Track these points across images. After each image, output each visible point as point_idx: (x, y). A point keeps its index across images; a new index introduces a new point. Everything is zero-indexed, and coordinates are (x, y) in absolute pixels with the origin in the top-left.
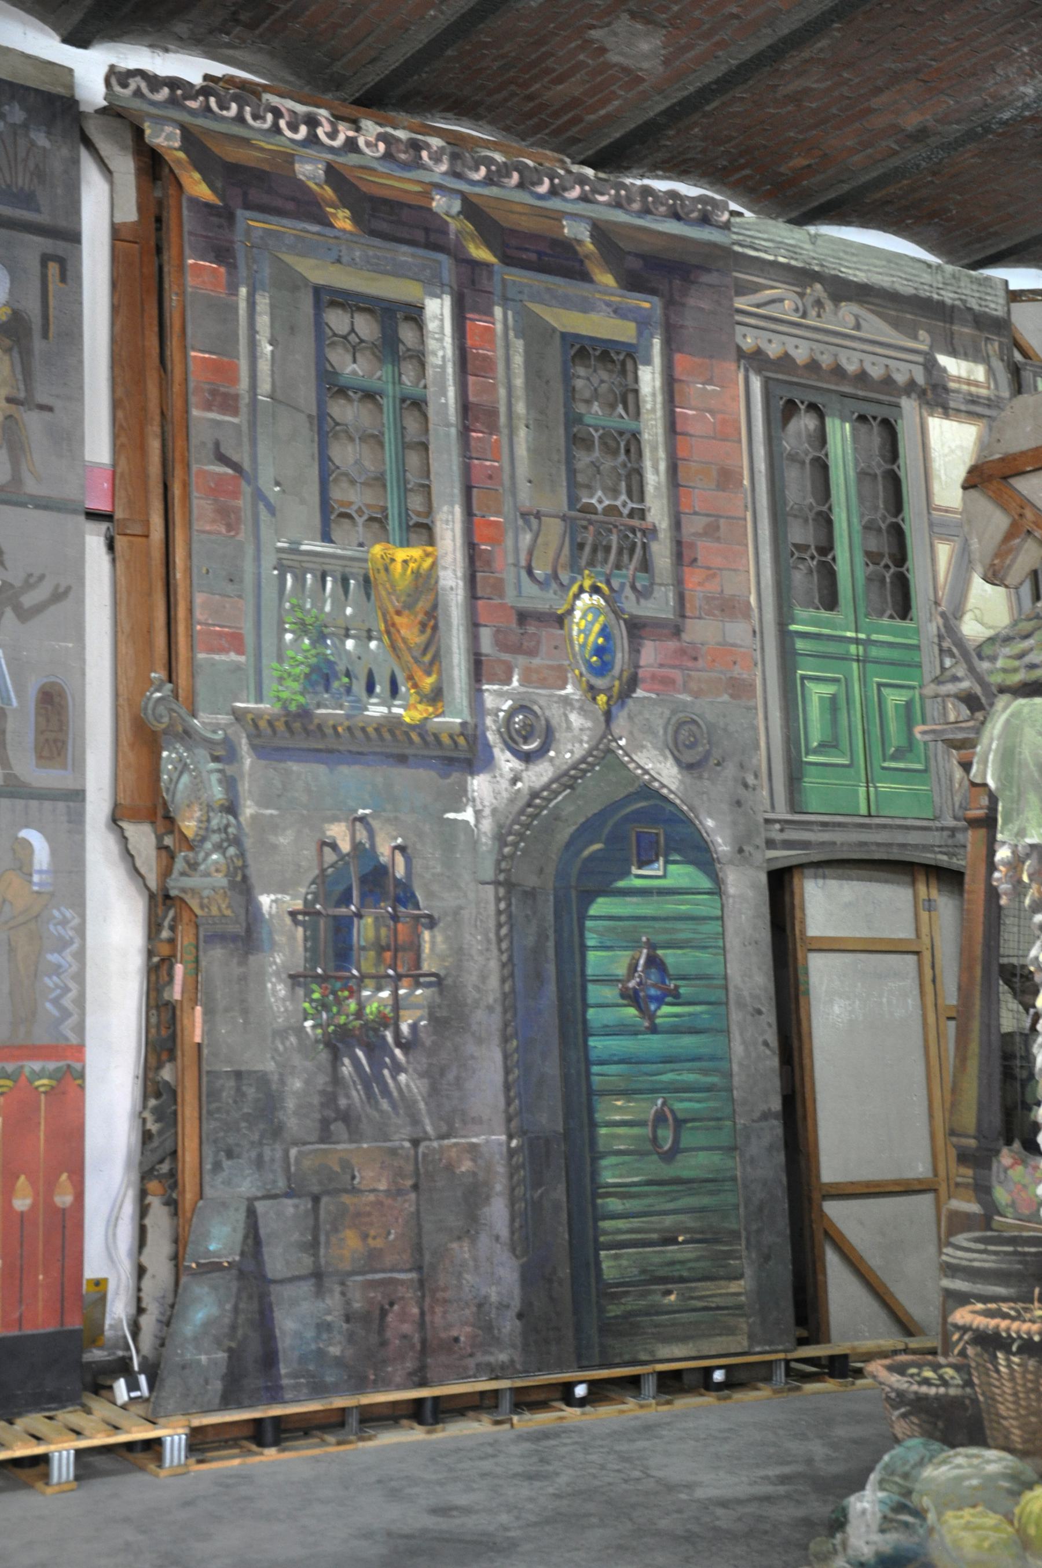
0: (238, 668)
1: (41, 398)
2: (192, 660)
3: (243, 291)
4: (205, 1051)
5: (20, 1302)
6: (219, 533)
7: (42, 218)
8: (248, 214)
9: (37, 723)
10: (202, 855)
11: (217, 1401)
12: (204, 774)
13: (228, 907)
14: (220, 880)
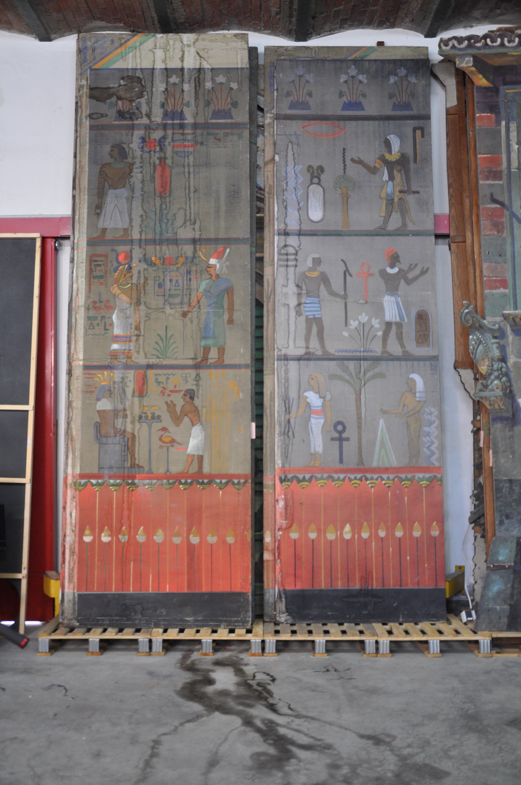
0: (504, 295)
1: (414, 189)
2: (482, 294)
3: (503, 123)
4: (494, 470)
5: (418, 575)
6: (494, 235)
7: (414, 112)
8: (506, 87)
9: (416, 328)
10: (489, 382)
11: (505, 627)
12: (490, 345)
13: (503, 405)
14: (499, 393)
